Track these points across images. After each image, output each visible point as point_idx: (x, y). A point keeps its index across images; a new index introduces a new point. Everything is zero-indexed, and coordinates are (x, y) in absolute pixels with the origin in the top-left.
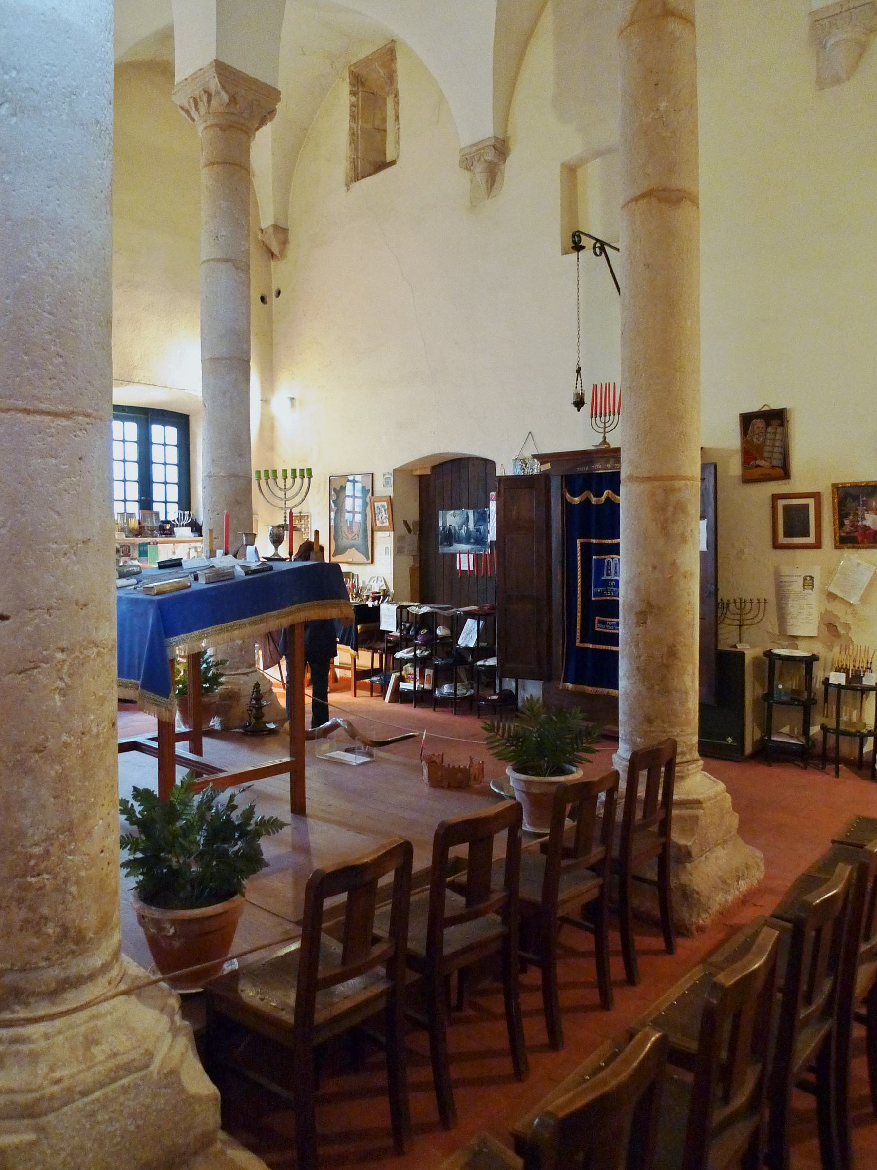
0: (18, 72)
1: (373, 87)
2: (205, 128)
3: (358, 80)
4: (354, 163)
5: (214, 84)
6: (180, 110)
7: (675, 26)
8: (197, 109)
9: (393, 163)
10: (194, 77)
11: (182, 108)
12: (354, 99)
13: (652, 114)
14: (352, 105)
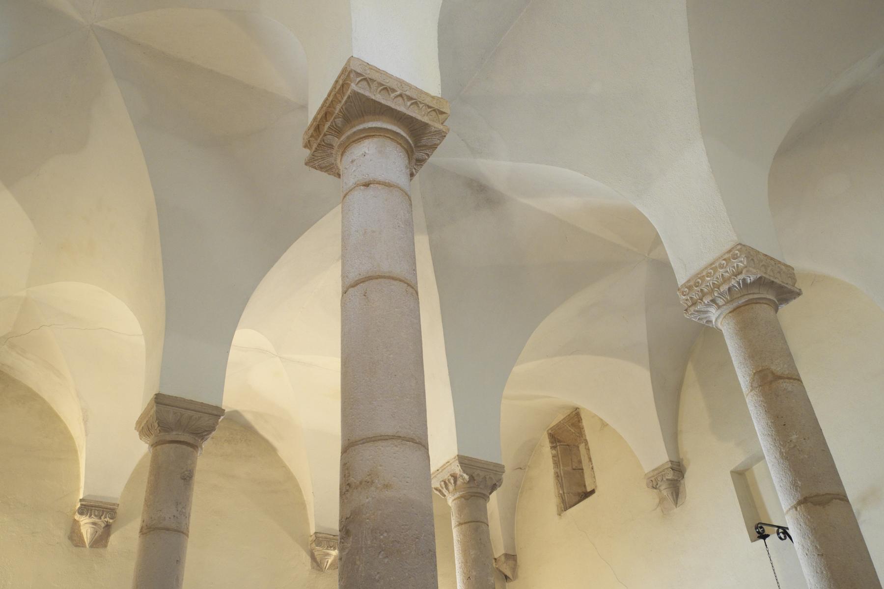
1: (567, 439)
3: (555, 438)
5: (458, 470)
8: (447, 489)
9: (593, 492)
10: (443, 467)
12: (554, 452)
14: (553, 456)
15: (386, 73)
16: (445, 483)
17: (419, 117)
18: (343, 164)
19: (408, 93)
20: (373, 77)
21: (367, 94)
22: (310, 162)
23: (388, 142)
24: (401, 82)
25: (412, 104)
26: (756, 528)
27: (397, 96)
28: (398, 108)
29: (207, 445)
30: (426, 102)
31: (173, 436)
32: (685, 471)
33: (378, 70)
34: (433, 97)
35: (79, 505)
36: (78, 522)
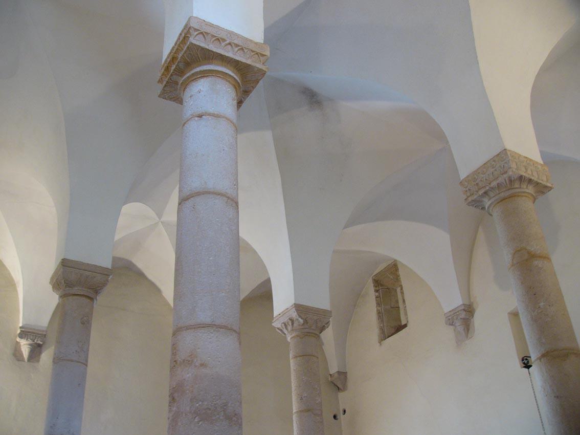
0: (202, 402)
2: (291, 338)
3: (377, 283)
4: (382, 330)
5: (294, 315)
6: (277, 330)
7: (538, 263)
8: (287, 329)
9: (405, 326)
10: (284, 313)
11: (278, 329)
12: (377, 294)
13: (537, 310)
15: (218, 27)
16: (285, 325)
17: (244, 60)
18: (186, 96)
19: (236, 42)
20: (208, 31)
21: (202, 45)
22: (163, 95)
23: (219, 80)
24: (231, 33)
25: (239, 50)
26: (523, 360)
27: (226, 45)
28: (227, 54)
29: (101, 299)
30: (250, 47)
31: (76, 290)
32: (474, 313)
33: (212, 25)
34: (256, 43)
35: (19, 331)
36: (19, 343)
